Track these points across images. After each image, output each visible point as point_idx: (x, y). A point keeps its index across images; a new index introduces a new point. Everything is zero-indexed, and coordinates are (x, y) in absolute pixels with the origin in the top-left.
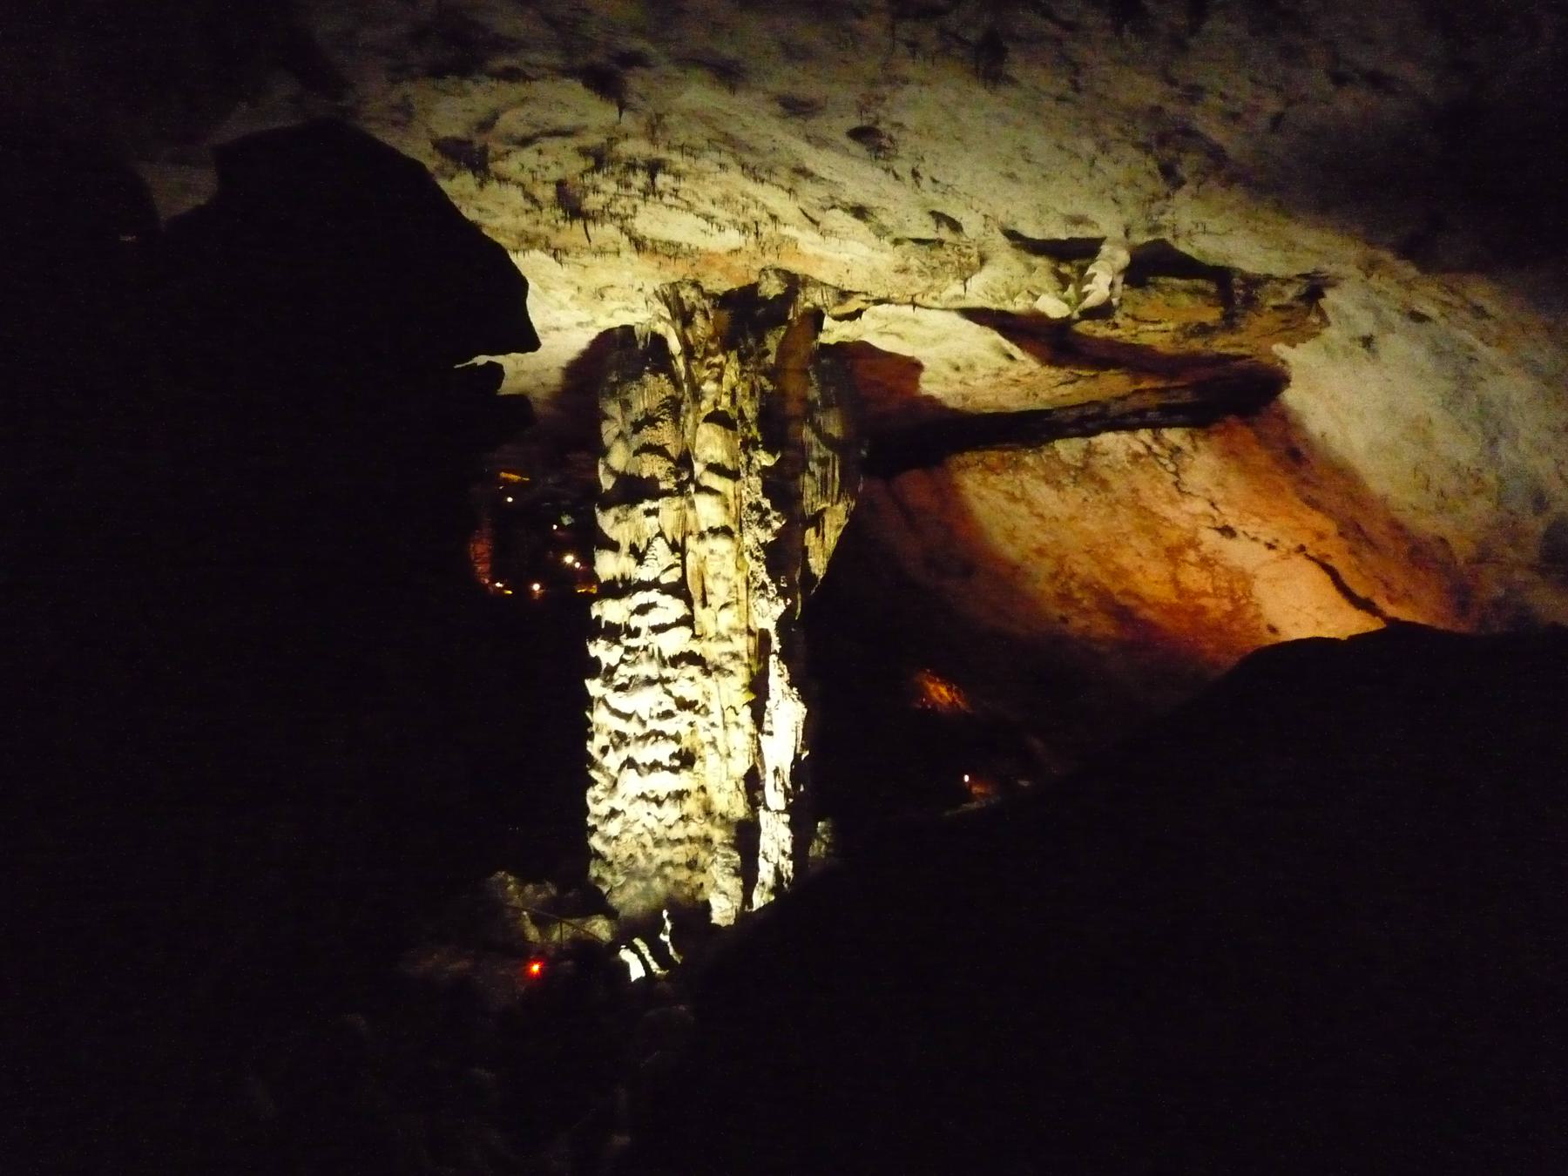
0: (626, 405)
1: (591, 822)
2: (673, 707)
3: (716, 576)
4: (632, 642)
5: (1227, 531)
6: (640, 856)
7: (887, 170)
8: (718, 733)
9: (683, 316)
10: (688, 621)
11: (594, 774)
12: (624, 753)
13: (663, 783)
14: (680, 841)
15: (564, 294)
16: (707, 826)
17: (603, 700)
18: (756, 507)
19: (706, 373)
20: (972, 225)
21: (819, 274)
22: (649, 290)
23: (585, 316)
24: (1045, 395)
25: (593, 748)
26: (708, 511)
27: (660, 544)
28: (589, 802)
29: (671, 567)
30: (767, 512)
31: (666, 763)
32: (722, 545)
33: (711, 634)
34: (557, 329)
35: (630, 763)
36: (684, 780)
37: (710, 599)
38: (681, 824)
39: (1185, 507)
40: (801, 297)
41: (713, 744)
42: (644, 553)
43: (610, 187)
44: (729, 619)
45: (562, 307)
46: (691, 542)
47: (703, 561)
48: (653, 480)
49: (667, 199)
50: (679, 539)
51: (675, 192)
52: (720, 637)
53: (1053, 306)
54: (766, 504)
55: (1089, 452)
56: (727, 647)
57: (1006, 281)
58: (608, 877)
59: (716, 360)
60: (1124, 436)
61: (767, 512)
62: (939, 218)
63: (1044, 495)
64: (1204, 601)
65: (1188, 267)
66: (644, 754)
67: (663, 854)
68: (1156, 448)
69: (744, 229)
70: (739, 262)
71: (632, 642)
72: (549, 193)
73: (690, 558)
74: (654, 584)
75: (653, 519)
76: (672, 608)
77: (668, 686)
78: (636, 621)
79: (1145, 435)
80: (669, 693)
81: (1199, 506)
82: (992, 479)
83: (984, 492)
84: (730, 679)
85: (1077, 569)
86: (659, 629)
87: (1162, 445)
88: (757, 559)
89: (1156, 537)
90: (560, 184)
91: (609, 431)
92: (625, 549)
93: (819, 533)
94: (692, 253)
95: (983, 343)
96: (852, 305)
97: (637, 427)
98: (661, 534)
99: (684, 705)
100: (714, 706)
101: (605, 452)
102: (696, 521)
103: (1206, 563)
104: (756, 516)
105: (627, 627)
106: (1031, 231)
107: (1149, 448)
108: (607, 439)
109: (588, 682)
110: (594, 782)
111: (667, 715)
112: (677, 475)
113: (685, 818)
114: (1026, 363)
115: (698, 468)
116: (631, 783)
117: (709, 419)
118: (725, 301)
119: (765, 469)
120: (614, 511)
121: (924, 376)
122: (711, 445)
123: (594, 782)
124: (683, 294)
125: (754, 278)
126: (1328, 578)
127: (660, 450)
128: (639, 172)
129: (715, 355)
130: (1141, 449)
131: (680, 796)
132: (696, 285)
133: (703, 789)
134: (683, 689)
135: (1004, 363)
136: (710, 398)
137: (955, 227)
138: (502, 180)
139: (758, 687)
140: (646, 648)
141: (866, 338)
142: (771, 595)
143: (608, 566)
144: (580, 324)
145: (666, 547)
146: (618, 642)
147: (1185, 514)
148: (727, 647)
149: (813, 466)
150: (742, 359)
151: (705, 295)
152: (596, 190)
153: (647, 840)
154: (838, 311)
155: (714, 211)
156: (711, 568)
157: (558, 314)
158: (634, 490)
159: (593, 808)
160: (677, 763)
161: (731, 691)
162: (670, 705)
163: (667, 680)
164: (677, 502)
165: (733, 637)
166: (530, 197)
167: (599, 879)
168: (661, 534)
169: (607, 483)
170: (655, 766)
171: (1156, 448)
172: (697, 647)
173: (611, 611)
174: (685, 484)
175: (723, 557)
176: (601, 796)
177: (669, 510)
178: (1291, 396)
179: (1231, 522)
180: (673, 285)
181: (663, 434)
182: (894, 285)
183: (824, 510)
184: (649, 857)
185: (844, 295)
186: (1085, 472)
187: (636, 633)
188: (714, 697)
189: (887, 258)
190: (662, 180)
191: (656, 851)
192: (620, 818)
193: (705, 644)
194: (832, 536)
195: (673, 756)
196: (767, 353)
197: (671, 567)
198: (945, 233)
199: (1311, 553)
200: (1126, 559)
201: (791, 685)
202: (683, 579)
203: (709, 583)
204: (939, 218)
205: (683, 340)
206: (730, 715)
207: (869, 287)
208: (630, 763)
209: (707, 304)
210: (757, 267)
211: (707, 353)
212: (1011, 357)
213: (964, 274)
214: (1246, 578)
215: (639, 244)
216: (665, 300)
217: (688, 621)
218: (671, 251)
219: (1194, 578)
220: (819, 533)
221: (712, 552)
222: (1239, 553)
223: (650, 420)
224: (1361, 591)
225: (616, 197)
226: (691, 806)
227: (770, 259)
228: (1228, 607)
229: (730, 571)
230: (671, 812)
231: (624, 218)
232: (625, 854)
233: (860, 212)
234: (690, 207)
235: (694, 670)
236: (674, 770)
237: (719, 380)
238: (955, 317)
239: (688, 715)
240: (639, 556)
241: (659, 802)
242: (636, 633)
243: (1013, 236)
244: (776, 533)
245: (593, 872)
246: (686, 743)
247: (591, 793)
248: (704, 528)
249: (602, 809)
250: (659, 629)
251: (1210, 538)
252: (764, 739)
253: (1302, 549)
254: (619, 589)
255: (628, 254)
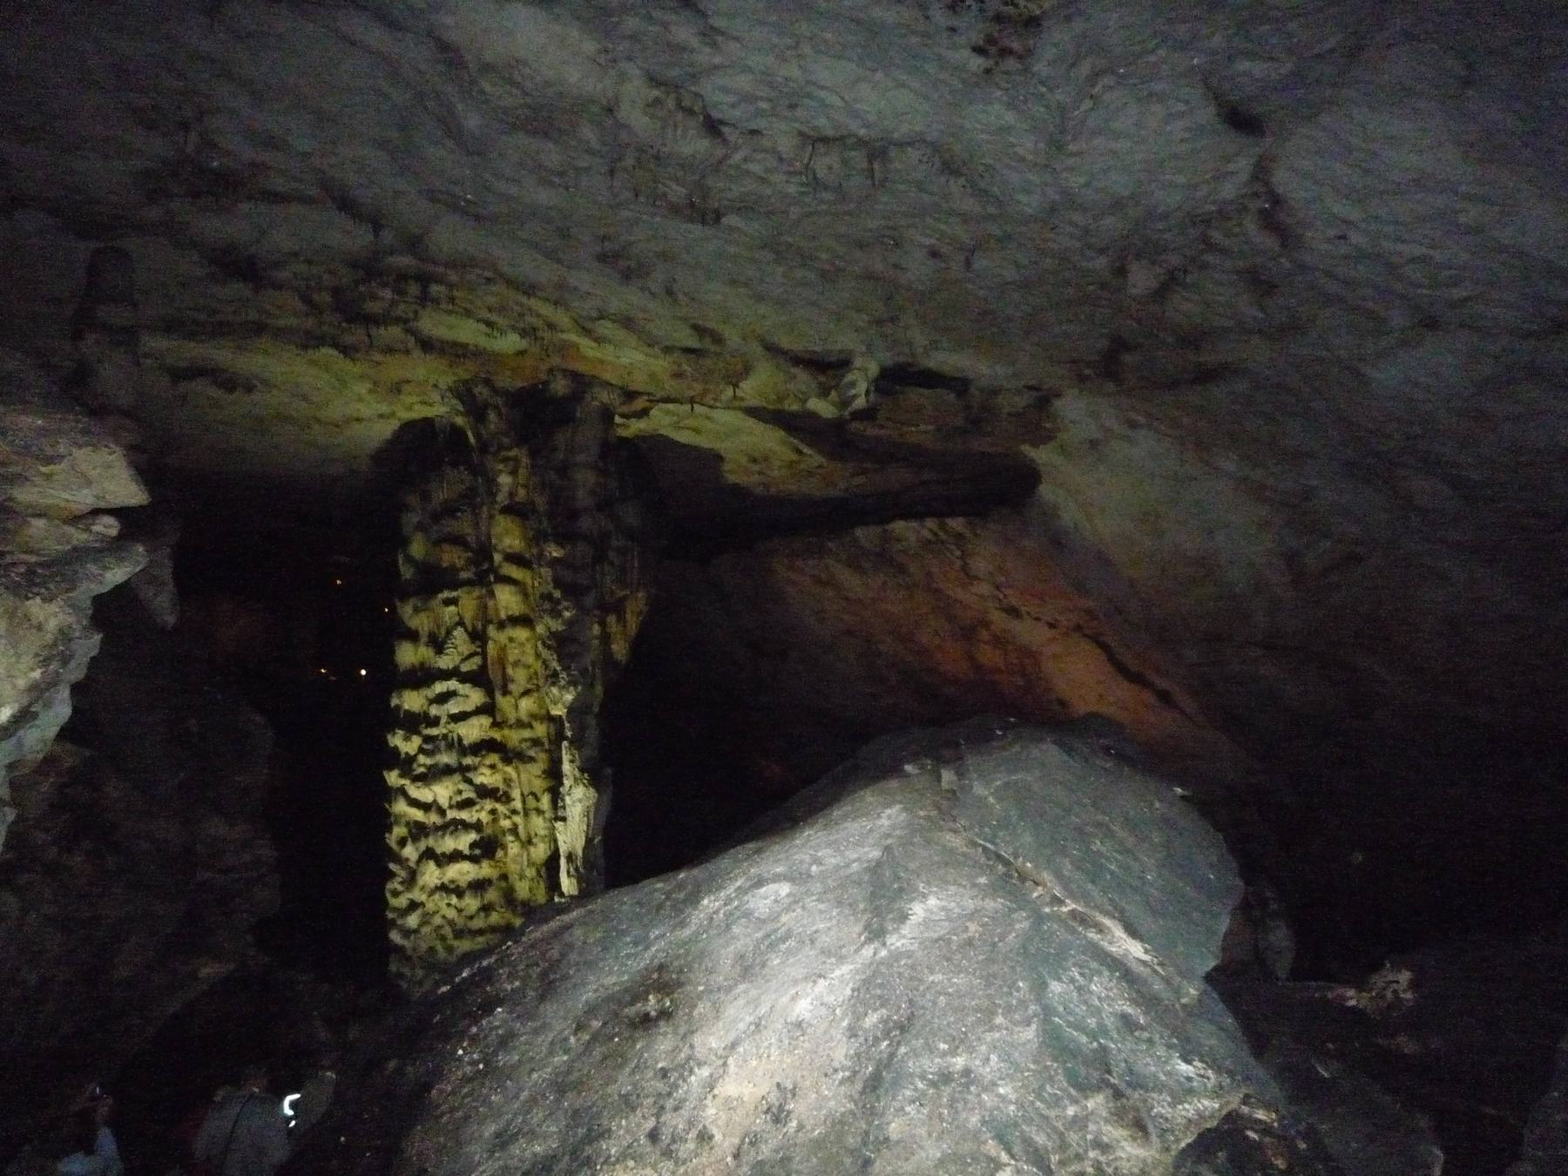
0: (426, 497)
1: (390, 915)
2: (472, 795)
3: (516, 664)
4: (434, 731)
5: (1014, 612)
6: (439, 948)
7: (642, 289)
8: (518, 819)
9: (477, 412)
10: (488, 709)
11: (392, 866)
12: (423, 845)
13: (462, 872)
14: (481, 932)
15: (362, 388)
16: (509, 915)
17: (402, 791)
18: (547, 597)
19: (501, 466)
20: (732, 337)
21: (607, 376)
22: (443, 386)
23: (384, 408)
24: (842, 485)
25: (392, 840)
26: (507, 600)
27: (459, 633)
28: (388, 895)
29: (471, 655)
30: (558, 602)
31: (467, 852)
32: (521, 634)
33: (512, 721)
34: (358, 420)
35: (429, 854)
36: (486, 870)
37: (512, 687)
38: (482, 914)
39: (974, 590)
40: (588, 397)
41: (514, 830)
42: (444, 642)
43: (387, 294)
44: (526, 705)
45: (360, 400)
46: (492, 631)
47: (503, 649)
48: (454, 569)
49: (443, 306)
50: (480, 627)
51: (452, 300)
52: (520, 724)
53: (823, 408)
54: (557, 594)
55: (887, 538)
56: (527, 734)
57: (759, 385)
58: (406, 971)
59: (512, 453)
60: (914, 524)
61: (558, 602)
62: (700, 330)
63: (846, 577)
64: (997, 677)
65: (931, 379)
66: (448, 844)
67: (465, 945)
68: (942, 535)
69: (523, 333)
70: (528, 362)
71: (434, 731)
72: (325, 298)
73: (491, 649)
74: (452, 674)
75: (452, 608)
76: (474, 697)
77: (470, 775)
78: (434, 711)
79: (931, 523)
80: (469, 782)
81: (984, 588)
82: (799, 563)
83: (793, 576)
84: (529, 766)
85: (882, 648)
86: (461, 717)
87: (946, 532)
88: (549, 648)
89: (951, 619)
90: (336, 292)
91: (412, 519)
92: (424, 639)
93: (621, 619)
94: (478, 353)
95: (770, 439)
96: (639, 404)
97: (436, 517)
98: (461, 623)
99: (485, 792)
100: (516, 794)
101: (404, 542)
102: (497, 610)
103: (999, 641)
104: (547, 605)
105: (426, 714)
106: (785, 342)
107: (936, 534)
108: (407, 530)
109: (385, 773)
110: (392, 875)
111: (467, 804)
112: (477, 564)
113: (486, 909)
114: (814, 458)
115: (497, 558)
116: (431, 875)
117: (507, 510)
118: (518, 399)
119: (556, 560)
120: (413, 601)
121: (726, 467)
122: (509, 537)
123: (392, 875)
124: (476, 391)
125: (543, 377)
126: (1104, 657)
127: (458, 541)
128: (411, 282)
129: (509, 449)
130: (930, 536)
131: (479, 886)
132: (487, 382)
133: (504, 877)
134: (485, 777)
135: (794, 457)
136: (505, 489)
137: (718, 340)
138: (279, 287)
139: (554, 774)
140: (445, 737)
141: (662, 432)
142: (563, 683)
143: (408, 655)
144: (381, 416)
145: (465, 636)
146: (418, 733)
147: (976, 596)
148: (527, 734)
149: (611, 554)
150: (533, 454)
151: (495, 391)
152: (374, 297)
153: (447, 931)
154: (625, 409)
155: (494, 317)
156: (513, 654)
157: (360, 406)
158: (433, 581)
159: (394, 902)
160: (477, 852)
161: (530, 776)
162: (469, 793)
163: (468, 768)
164: (477, 592)
165: (535, 724)
166: (306, 299)
167: (401, 975)
168: (461, 623)
169: (407, 572)
170: (456, 856)
171: (942, 535)
172: (497, 735)
173: (412, 701)
174: (485, 577)
175: (522, 645)
176: (400, 888)
177: (468, 603)
178: (1046, 491)
179: (1014, 602)
180: (465, 382)
181: (462, 525)
182: (671, 387)
183: (625, 598)
184: (450, 949)
185: (630, 395)
186: (885, 558)
187: (435, 722)
188: (515, 784)
189: (662, 365)
190: (436, 289)
191: (456, 943)
192: (419, 912)
193: (506, 732)
194: (633, 623)
195: (473, 846)
196: (555, 449)
197: (471, 655)
198: (707, 344)
199: (1087, 631)
200: (924, 638)
201: (582, 770)
202: (483, 667)
203: (510, 671)
204: (700, 330)
205: (478, 436)
206: (531, 802)
207: (651, 389)
208: (429, 854)
209: (500, 401)
210: (544, 367)
211: (501, 448)
212: (799, 452)
213: (734, 380)
214: (1027, 653)
215: (427, 345)
216: (459, 397)
217: (488, 709)
218: (455, 352)
219: (988, 656)
220: (621, 619)
221: (511, 640)
222: (1029, 633)
223: (449, 510)
224: (1133, 665)
225: (393, 303)
226: (492, 895)
227: (556, 360)
228: (1020, 682)
229: (531, 660)
230: (471, 903)
231: (406, 321)
232: (424, 946)
233: (627, 323)
234: (468, 314)
235: (494, 758)
236: (474, 859)
237: (514, 473)
238: (740, 415)
239: (489, 804)
240: (438, 646)
241: (460, 893)
242: (435, 722)
243: (772, 349)
244: (570, 623)
245: (393, 968)
246: (488, 831)
247: (390, 886)
248: (503, 616)
249: (402, 902)
250: (461, 717)
251: (997, 617)
252: (559, 825)
253: (1078, 628)
254: (422, 677)
255: (417, 353)
